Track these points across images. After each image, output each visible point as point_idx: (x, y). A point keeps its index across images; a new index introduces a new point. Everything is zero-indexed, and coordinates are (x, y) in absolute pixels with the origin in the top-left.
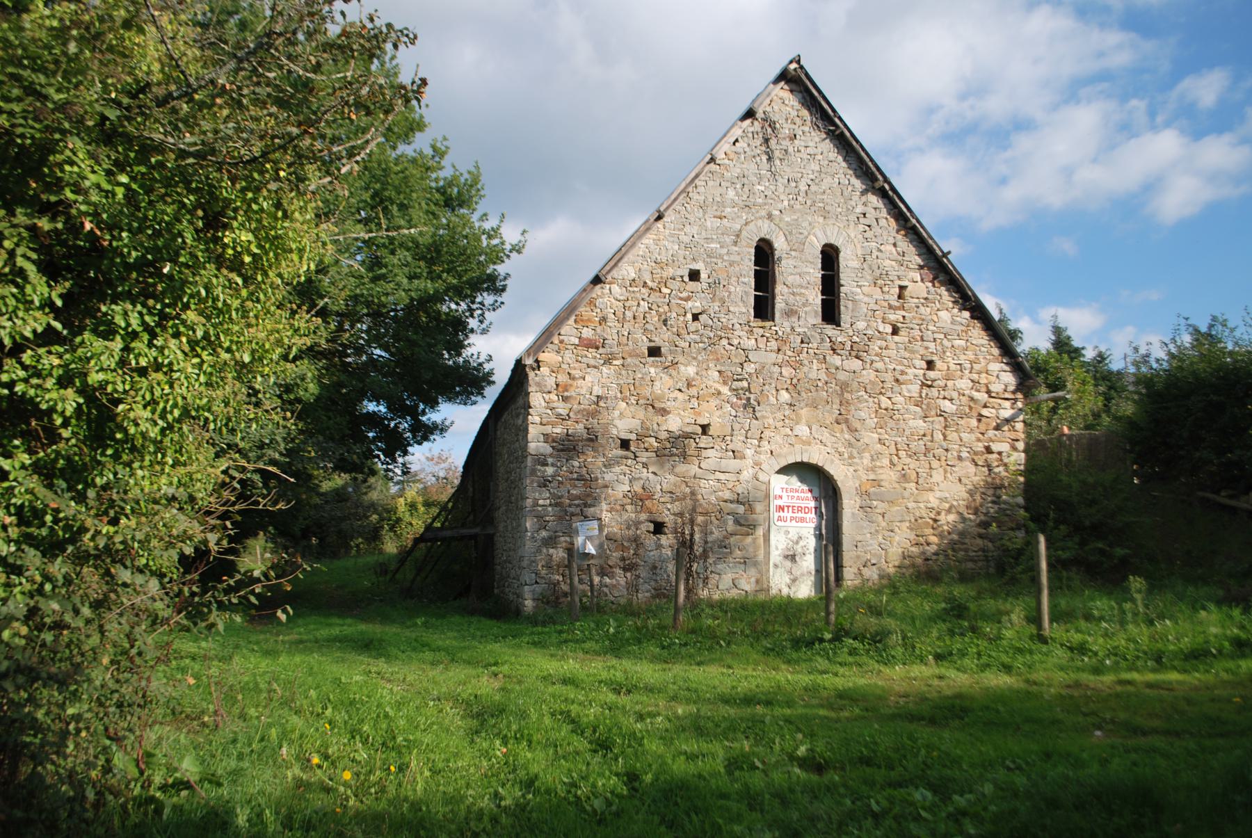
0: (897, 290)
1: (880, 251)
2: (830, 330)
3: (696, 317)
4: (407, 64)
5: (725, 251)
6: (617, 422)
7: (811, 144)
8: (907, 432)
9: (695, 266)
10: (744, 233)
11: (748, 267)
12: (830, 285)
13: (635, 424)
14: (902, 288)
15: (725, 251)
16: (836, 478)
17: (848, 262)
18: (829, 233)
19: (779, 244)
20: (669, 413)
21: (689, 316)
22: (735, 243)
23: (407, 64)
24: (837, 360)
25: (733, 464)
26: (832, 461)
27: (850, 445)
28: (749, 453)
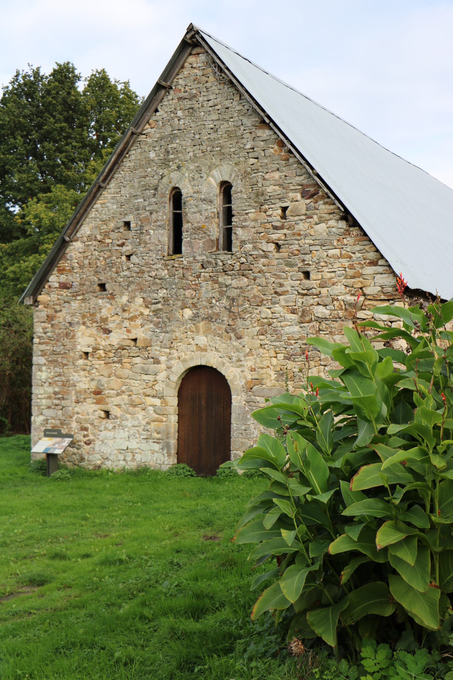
0: (280, 211)
1: (264, 179)
3: (128, 257)
4: (85, 71)
6: (80, 340)
7: (211, 97)
8: (285, 338)
9: (126, 220)
10: (161, 186)
11: (166, 213)
13: (91, 341)
14: (284, 209)
15: (147, 203)
16: (226, 377)
17: (238, 187)
20: (110, 332)
21: (124, 258)
23: (85, 71)
26: (224, 364)
27: (238, 350)
28: (163, 359)
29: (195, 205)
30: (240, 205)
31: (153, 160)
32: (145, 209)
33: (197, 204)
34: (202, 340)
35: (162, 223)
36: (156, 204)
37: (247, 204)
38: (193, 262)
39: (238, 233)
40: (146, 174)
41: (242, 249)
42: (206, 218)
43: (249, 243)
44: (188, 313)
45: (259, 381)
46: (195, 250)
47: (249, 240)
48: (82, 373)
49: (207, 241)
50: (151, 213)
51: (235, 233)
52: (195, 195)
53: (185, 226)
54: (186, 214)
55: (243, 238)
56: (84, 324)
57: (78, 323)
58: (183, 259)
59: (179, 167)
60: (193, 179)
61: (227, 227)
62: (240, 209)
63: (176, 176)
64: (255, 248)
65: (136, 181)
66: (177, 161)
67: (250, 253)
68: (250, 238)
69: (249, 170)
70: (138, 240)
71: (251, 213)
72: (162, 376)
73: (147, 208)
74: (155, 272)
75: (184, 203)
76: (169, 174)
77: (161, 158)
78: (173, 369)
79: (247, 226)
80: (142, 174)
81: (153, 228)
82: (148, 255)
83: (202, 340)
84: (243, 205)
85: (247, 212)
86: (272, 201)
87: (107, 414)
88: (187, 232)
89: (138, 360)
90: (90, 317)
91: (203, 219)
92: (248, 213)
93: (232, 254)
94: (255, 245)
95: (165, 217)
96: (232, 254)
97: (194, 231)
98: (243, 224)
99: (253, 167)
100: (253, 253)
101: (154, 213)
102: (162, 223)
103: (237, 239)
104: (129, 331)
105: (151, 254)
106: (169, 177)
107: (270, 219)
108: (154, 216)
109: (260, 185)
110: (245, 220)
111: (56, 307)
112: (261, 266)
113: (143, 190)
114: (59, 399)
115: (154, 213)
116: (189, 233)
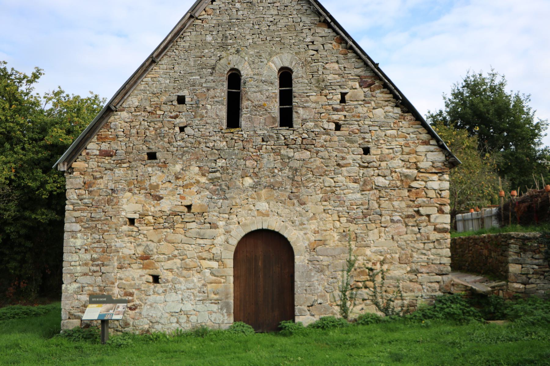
2: (285, 131)
9: (181, 93)
12: (286, 97)
13: (139, 208)
17: (298, 73)
19: (246, 71)
20: (162, 198)
22: (212, 74)
25: (210, 232)
28: (221, 224)
30: (301, 88)
31: (209, 43)
32: (202, 86)
33: (257, 84)
34: (263, 206)
35: (220, 99)
36: (214, 82)
38: (253, 136)
39: (299, 112)
40: (203, 54)
42: (267, 98)
44: (248, 181)
45: (323, 242)
46: (255, 125)
47: (310, 118)
48: (126, 239)
49: (268, 117)
50: (208, 90)
51: (297, 112)
52: (255, 77)
53: (245, 104)
54: (247, 93)
55: (305, 117)
56: (130, 191)
57: (123, 190)
58: (243, 133)
59: (238, 51)
60: (253, 63)
63: (235, 59)
64: (316, 126)
66: (235, 46)
67: (312, 130)
68: (312, 117)
69: (309, 59)
70: (193, 113)
72: (220, 240)
73: (204, 85)
74: (213, 144)
76: (228, 56)
77: (218, 41)
78: (232, 233)
80: (199, 54)
82: (204, 127)
83: (263, 206)
85: (308, 94)
86: (333, 87)
87: (156, 279)
88: (247, 108)
89: (193, 225)
90: (136, 185)
91: (264, 98)
93: (294, 130)
94: (316, 123)
95: (223, 94)
96: (294, 130)
98: (305, 104)
99: (314, 58)
100: (315, 130)
101: (212, 90)
102: (220, 99)
103: (299, 117)
104: (183, 198)
106: (227, 59)
107: (331, 102)
108: (212, 92)
109: (320, 73)
110: (307, 102)
111: (95, 174)
112: (322, 141)
113: (199, 69)
114: (98, 265)
115: (212, 90)
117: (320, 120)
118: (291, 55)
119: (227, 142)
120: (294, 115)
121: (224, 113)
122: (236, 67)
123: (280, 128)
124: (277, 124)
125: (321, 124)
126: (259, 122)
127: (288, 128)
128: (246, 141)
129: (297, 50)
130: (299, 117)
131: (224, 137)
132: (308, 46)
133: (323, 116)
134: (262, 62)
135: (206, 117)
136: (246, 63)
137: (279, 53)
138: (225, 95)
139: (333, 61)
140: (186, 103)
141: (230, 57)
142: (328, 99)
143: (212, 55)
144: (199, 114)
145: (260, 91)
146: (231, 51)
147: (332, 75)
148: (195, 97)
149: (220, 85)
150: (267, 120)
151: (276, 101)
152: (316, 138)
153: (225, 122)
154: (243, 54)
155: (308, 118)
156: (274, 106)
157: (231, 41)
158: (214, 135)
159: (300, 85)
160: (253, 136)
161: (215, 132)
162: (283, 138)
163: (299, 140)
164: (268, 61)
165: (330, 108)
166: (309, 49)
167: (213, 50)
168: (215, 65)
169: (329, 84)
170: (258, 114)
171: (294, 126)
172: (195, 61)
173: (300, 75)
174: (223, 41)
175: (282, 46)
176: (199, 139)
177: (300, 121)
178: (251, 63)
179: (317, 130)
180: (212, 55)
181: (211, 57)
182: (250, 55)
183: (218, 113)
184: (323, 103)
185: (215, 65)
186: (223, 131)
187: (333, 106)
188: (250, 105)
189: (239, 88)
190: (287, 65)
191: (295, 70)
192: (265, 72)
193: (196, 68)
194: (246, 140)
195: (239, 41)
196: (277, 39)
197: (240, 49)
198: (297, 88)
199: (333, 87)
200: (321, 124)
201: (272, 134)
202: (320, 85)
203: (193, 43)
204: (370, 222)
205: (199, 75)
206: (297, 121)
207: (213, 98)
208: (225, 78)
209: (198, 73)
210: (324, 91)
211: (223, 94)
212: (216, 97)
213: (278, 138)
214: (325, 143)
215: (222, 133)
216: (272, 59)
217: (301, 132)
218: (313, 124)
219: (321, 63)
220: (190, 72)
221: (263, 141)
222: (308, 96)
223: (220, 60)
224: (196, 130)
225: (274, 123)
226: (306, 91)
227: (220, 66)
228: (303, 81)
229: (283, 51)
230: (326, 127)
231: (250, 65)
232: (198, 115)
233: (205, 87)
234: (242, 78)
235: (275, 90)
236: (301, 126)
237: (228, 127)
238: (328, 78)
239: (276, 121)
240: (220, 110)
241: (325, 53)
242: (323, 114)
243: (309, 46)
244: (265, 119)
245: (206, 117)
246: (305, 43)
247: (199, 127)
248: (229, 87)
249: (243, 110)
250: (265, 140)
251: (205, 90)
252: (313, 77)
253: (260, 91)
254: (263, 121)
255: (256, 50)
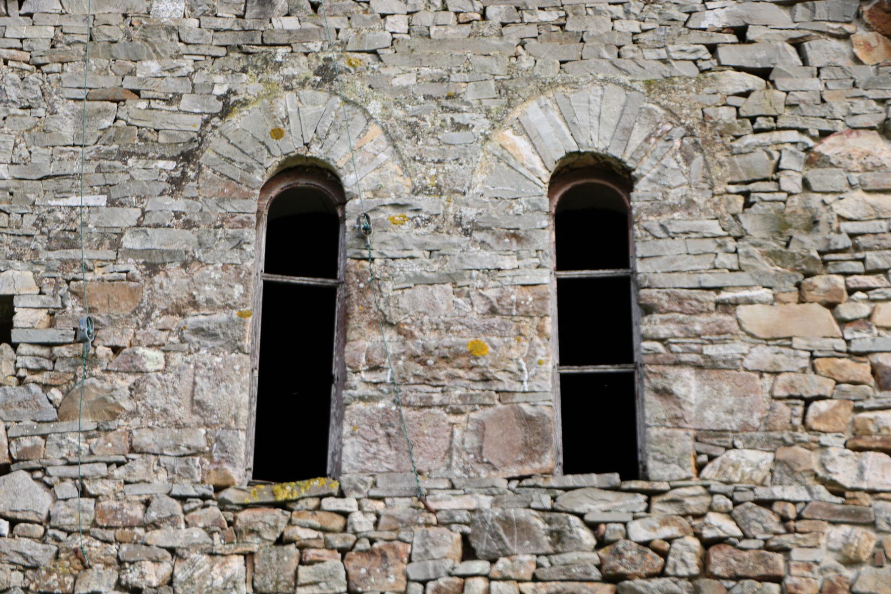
1: (813, 160)
2: (596, 497)
5: (130, 215)
10: (216, 145)
11: (235, 277)
12: (598, 318)
15: (130, 215)
17: (665, 186)
18: (582, 117)
19: (368, 171)
22: (177, 183)
24: (61, 227)
29: (422, 246)
30: (684, 263)
31: (170, 30)
32: (116, 245)
33: (435, 242)
35: (221, 317)
36: (189, 225)
37: (730, 261)
38: (409, 524)
39: (678, 389)
40: (130, 83)
41: (707, 472)
42: (493, 311)
43: (750, 444)
46: (421, 463)
47: (745, 427)
49: (498, 419)
50: (152, 268)
51: (665, 393)
52: (425, 203)
53: (361, 343)
54: (374, 284)
55: (712, 418)
58: (349, 504)
59: (327, 74)
60: (414, 130)
61: (575, 370)
62: (693, 282)
63: (309, 111)
64: (785, 469)
65: (61, 109)
66: (315, 46)
67: (762, 493)
68: (755, 421)
69: (726, 115)
70: (56, 394)
71: (750, 302)
73: (129, 242)
74: (165, 569)
75: (363, 234)
76: (271, 95)
77: (219, 23)
79: (732, 364)
80: (109, 82)
81: (162, 337)
82: (119, 473)
84: (703, 264)
85: (725, 295)
86: (870, 256)
88: (375, 368)
91: (475, 312)
92: (736, 303)
93: (651, 494)
94: (784, 453)
95: (238, 289)
96: (651, 494)
97: (420, 369)
98: (709, 350)
99: (749, 107)
100: (778, 492)
101: (173, 268)
102: (221, 317)
103: (677, 421)
105: (139, 467)
106: (269, 112)
107: (862, 340)
108: (173, 282)
109: (791, 182)
110: (721, 335)
112: (829, 560)
113: (107, 155)
115: (173, 268)
116: (386, 376)
117: (806, 436)
118: (617, 96)
119: (249, 556)
120: (651, 409)
121: (237, 392)
122: (316, 151)
123: (571, 480)
124: (552, 458)
125: (813, 460)
126: (443, 444)
127: (615, 478)
128: (370, 553)
129: (656, 71)
130: (677, 421)
131: (236, 532)
132: (712, 49)
133: (819, 417)
134: (458, 127)
135: (134, 414)
136: (375, 131)
137: (553, 85)
138: (248, 296)
139: (859, 121)
140: (15, 336)
141: (286, 103)
142: (843, 322)
143: (183, 87)
144: (93, 396)
145: (452, 278)
146: (288, 71)
147: (859, 194)
148: (73, 306)
149: (223, 245)
150: (493, 432)
151: (541, 331)
152: (787, 540)
153: (243, 443)
154: (357, 87)
155: (732, 423)
156: (529, 358)
157: (291, 23)
158: (172, 519)
159: (678, 245)
160: (409, 524)
161: (183, 499)
162: (587, 538)
163: (687, 553)
164: (497, 123)
165: (862, 370)
166: (722, 67)
167: (187, 64)
168: (201, 139)
169: (843, 241)
170: (437, 398)
171: (654, 468)
172: (83, 118)
173: (674, 196)
174: (249, 23)
175: (572, 50)
176: (79, 541)
177: (685, 442)
178: (401, 131)
179: (791, 492)
180: (183, 87)
181: (178, 97)
182: (395, 90)
183: (206, 394)
184: (817, 343)
185: (201, 139)
186: (229, 494)
187: (880, 358)
188: (392, 349)
189: (331, 270)
190: (599, 140)
191: (645, 170)
192: (479, 177)
193: (90, 152)
194: (364, 545)
195: (333, 22)
196: (543, 16)
197: (342, 64)
198: (660, 261)
199: (870, 256)
200: (813, 460)
201: (523, 513)
202: (794, 248)
203: (78, 28)
204: (349, 529)
205: (106, 188)
206: (667, 440)
207: (178, 311)
208: (253, 206)
209: (99, 179)
210: (818, 281)
211: (238, 289)
212: (194, 304)
213: (558, 537)
214: (849, 574)
215: (223, 505)
216: (515, 113)
217: (694, 505)
218: (764, 458)
219: (794, 136)
220: (50, 171)
221: (468, 553)
222: (726, 307)
223: (226, 112)
224: (68, 489)
225: (531, 451)
226: (712, 280)
227: (224, 147)
228: (695, 224)
229: (574, 71)
230: (845, 475)
231: (393, 141)
232: (82, 404)
233: (131, 252)
234: (350, 206)
235: (536, 271)
236: (691, 471)
237: (255, 476)
238: (840, 208)
239: (546, 438)
240: (219, 378)
241: (816, 84)
242: (822, 406)
243: (722, 52)
244: (481, 429)
245: (134, 414)
246: (695, 36)
247: (84, 470)
248: (274, 261)
249: (354, 380)
250: (480, 546)
251: (131, 265)
252: (748, 205)
253: (452, 278)
254: (471, 441)
255: (425, 71)
